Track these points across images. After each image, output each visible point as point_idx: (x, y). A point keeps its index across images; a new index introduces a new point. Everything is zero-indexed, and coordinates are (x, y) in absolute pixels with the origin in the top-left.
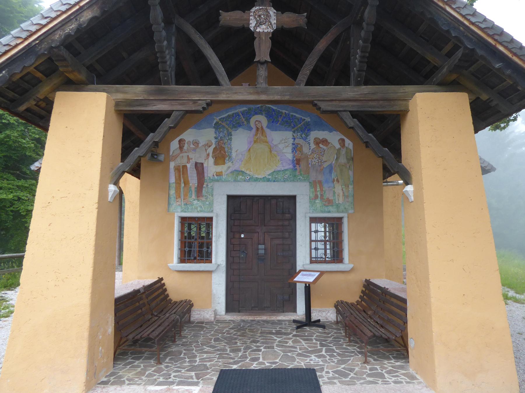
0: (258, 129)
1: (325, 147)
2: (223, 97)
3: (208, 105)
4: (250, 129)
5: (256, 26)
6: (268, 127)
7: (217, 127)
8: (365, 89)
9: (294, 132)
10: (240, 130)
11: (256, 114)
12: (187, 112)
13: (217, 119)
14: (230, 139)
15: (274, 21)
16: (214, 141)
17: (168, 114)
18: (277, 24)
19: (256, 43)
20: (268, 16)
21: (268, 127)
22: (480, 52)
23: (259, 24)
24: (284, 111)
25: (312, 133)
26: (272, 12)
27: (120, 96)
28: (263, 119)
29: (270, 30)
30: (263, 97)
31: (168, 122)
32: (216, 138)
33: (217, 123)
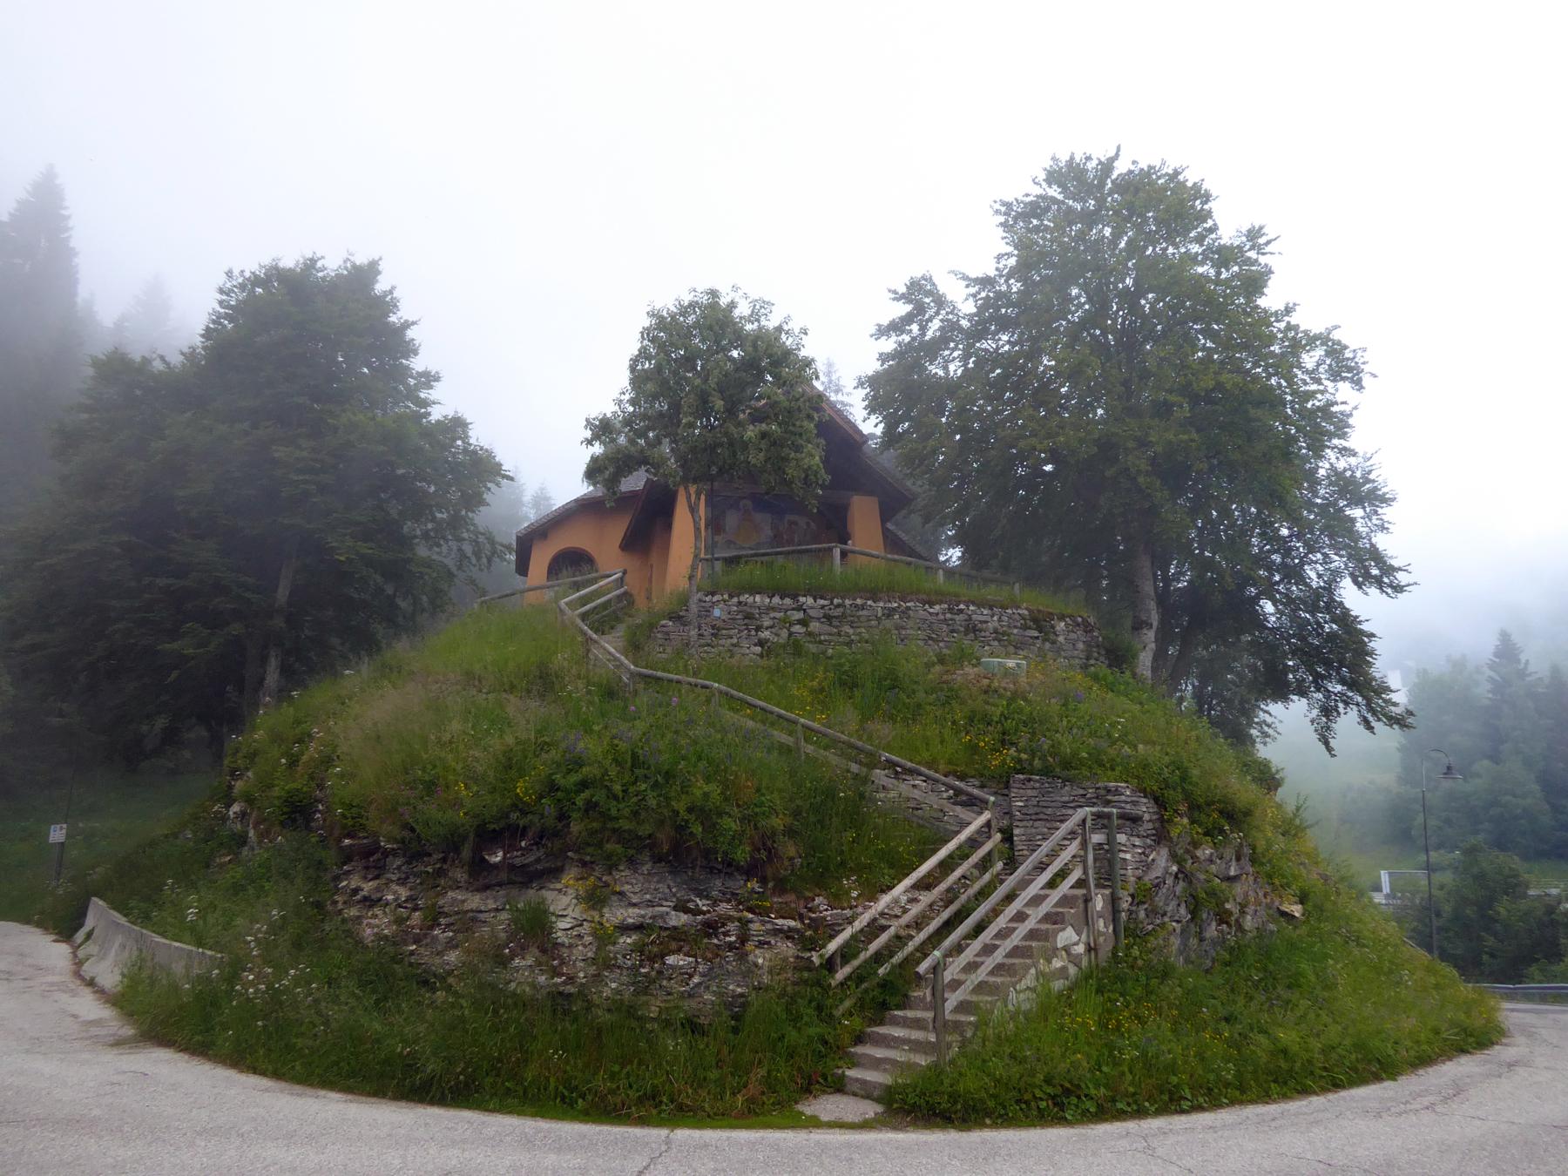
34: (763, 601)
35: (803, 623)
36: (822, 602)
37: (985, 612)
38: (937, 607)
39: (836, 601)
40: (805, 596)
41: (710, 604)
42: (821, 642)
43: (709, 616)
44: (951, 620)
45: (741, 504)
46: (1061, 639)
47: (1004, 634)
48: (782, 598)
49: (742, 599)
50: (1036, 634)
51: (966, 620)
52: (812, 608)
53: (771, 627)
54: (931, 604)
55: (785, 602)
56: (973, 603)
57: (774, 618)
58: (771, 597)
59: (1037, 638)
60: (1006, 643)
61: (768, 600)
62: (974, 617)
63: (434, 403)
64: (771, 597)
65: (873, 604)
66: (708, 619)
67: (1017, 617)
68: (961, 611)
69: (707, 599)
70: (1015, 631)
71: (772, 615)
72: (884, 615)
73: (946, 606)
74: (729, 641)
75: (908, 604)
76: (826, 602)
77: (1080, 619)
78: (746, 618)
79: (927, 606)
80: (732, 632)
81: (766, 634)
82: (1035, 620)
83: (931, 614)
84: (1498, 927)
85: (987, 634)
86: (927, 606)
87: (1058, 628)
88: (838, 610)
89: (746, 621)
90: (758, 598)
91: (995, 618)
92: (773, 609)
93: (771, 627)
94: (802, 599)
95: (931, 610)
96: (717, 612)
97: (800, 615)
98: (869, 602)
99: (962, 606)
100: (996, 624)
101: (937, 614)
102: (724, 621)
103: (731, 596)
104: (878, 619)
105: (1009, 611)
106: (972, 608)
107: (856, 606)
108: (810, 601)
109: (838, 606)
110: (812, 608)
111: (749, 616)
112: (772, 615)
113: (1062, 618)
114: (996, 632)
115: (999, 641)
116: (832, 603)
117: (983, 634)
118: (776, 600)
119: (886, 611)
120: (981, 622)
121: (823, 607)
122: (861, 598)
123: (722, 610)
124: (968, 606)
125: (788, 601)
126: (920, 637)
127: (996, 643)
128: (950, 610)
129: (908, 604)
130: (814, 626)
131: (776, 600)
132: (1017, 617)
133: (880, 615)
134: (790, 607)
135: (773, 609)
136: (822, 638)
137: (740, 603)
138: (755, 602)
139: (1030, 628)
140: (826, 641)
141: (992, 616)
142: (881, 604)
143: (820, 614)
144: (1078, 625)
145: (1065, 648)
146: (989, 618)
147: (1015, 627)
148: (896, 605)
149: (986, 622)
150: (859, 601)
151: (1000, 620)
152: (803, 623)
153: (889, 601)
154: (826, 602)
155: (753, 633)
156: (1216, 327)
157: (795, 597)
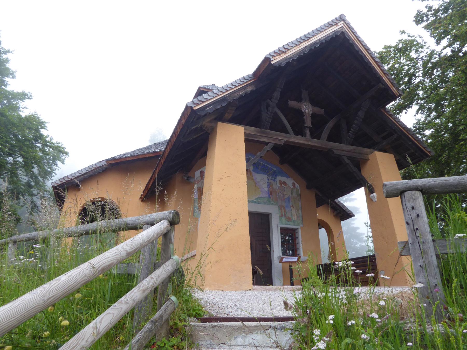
6: (253, 171)
9: (268, 175)
21: (253, 171)
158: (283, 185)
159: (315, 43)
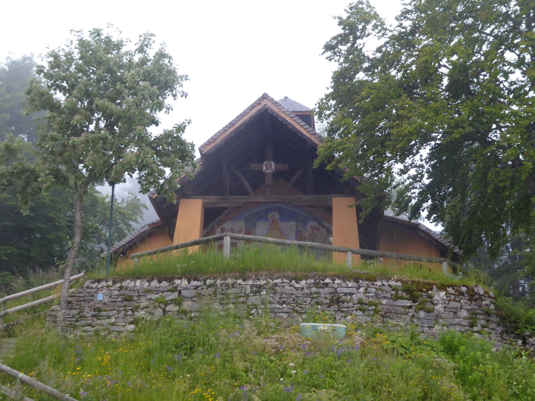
0: (273, 221)
1: (317, 232)
2: (250, 200)
3: (244, 204)
4: (268, 221)
5: (266, 170)
6: (280, 219)
7: (246, 220)
8: (313, 196)
9: (297, 222)
10: (261, 222)
11: (272, 211)
12: (235, 207)
13: (246, 215)
14: (255, 227)
15: (273, 167)
16: (244, 229)
17: (226, 208)
18: (275, 169)
19: (266, 177)
20: (271, 165)
21: (280, 219)
22: (351, 182)
23: (267, 169)
24: (290, 209)
25: (309, 223)
26: (273, 164)
27: (206, 201)
28: (276, 215)
29: (272, 172)
30: (269, 200)
31: (226, 211)
32: (245, 227)
33: (246, 217)
34: (142, 284)
35: (177, 302)
36: (195, 283)
37: (350, 285)
38: (303, 282)
39: (208, 282)
40: (180, 278)
41: (95, 290)
42: (191, 319)
43: (93, 300)
44: (316, 293)
45: (270, 216)
46: (439, 308)
47: (370, 304)
48: (160, 282)
49: (125, 284)
50: (408, 303)
51: (332, 293)
52: (186, 289)
53: (147, 307)
54: (298, 280)
55: (162, 284)
56: (339, 278)
57: (151, 299)
58: (149, 281)
59: (410, 307)
60: (372, 313)
61: (147, 284)
62: (339, 290)
63: (324, 52)
64: (149, 281)
65: (243, 283)
66: (91, 303)
67: (387, 288)
68: (327, 285)
69: (94, 286)
70: (384, 301)
71: (149, 297)
72: (251, 292)
73: (312, 281)
74: (108, 320)
75: (275, 281)
76: (199, 283)
77: (464, 289)
78: (126, 300)
79: (293, 281)
80: (111, 313)
81: (141, 313)
82: (408, 291)
83: (297, 289)
84: (169, 302)
85: (351, 304)
86: (293, 281)
87: (436, 297)
88: (210, 289)
89: (125, 303)
90: (138, 283)
91: (362, 290)
92: (149, 291)
93: (147, 307)
94: (177, 282)
95: (297, 286)
96: (100, 297)
97: (175, 295)
98: (240, 281)
99: (328, 280)
100: (361, 296)
101: (302, 289)
102: (105, 304)
103: (115, 283)
104: (247, 296)
105: (379, 283)
106: (337, 281)
107: (227, 285)
108: (185, 282)
109: (210, 286)
110: (186, 289)
111: (128, 299)
112: (149, 297)
113: (442, 287)
114: (360, 302)
115: (363, 311)
116: (205, 284)
117: (346, 305)
118: (155, 283)
119: (254, 289)
120: (346, 294)
121: (196, 288)
122: (232, 278)
123: (104, 294)
124: (333, 280)
125: (165, 284)
126: (285, 310)
127: (359, 313)
128: (316, 285)
129: (275, 281)
130: (187, 305)
131: (155, 283)
132: (387, 288)
133: (248, 292)
134: (166, 289)
135: (149, 291)
136: (193, 314)
137: (121, 288)
138: (135, 286)
139: (402, 298)
140: (195, 317)
141: (358, 288)
142: (250, 282)
143: (193, 293)
144: (462, 294)
145: (443, 316)
146: (354, 290)
147: (385, 298)
148: (264, 282)
149: (351, 294)
150: (230, 281)
151: (366, 291)
152: (177, 302)
153: (258, 279)
154: (199, 283)
155: (130, 313)
156: (532, 14)
157: (170, 280)
158: (314, 231)
159: (241, 126)
